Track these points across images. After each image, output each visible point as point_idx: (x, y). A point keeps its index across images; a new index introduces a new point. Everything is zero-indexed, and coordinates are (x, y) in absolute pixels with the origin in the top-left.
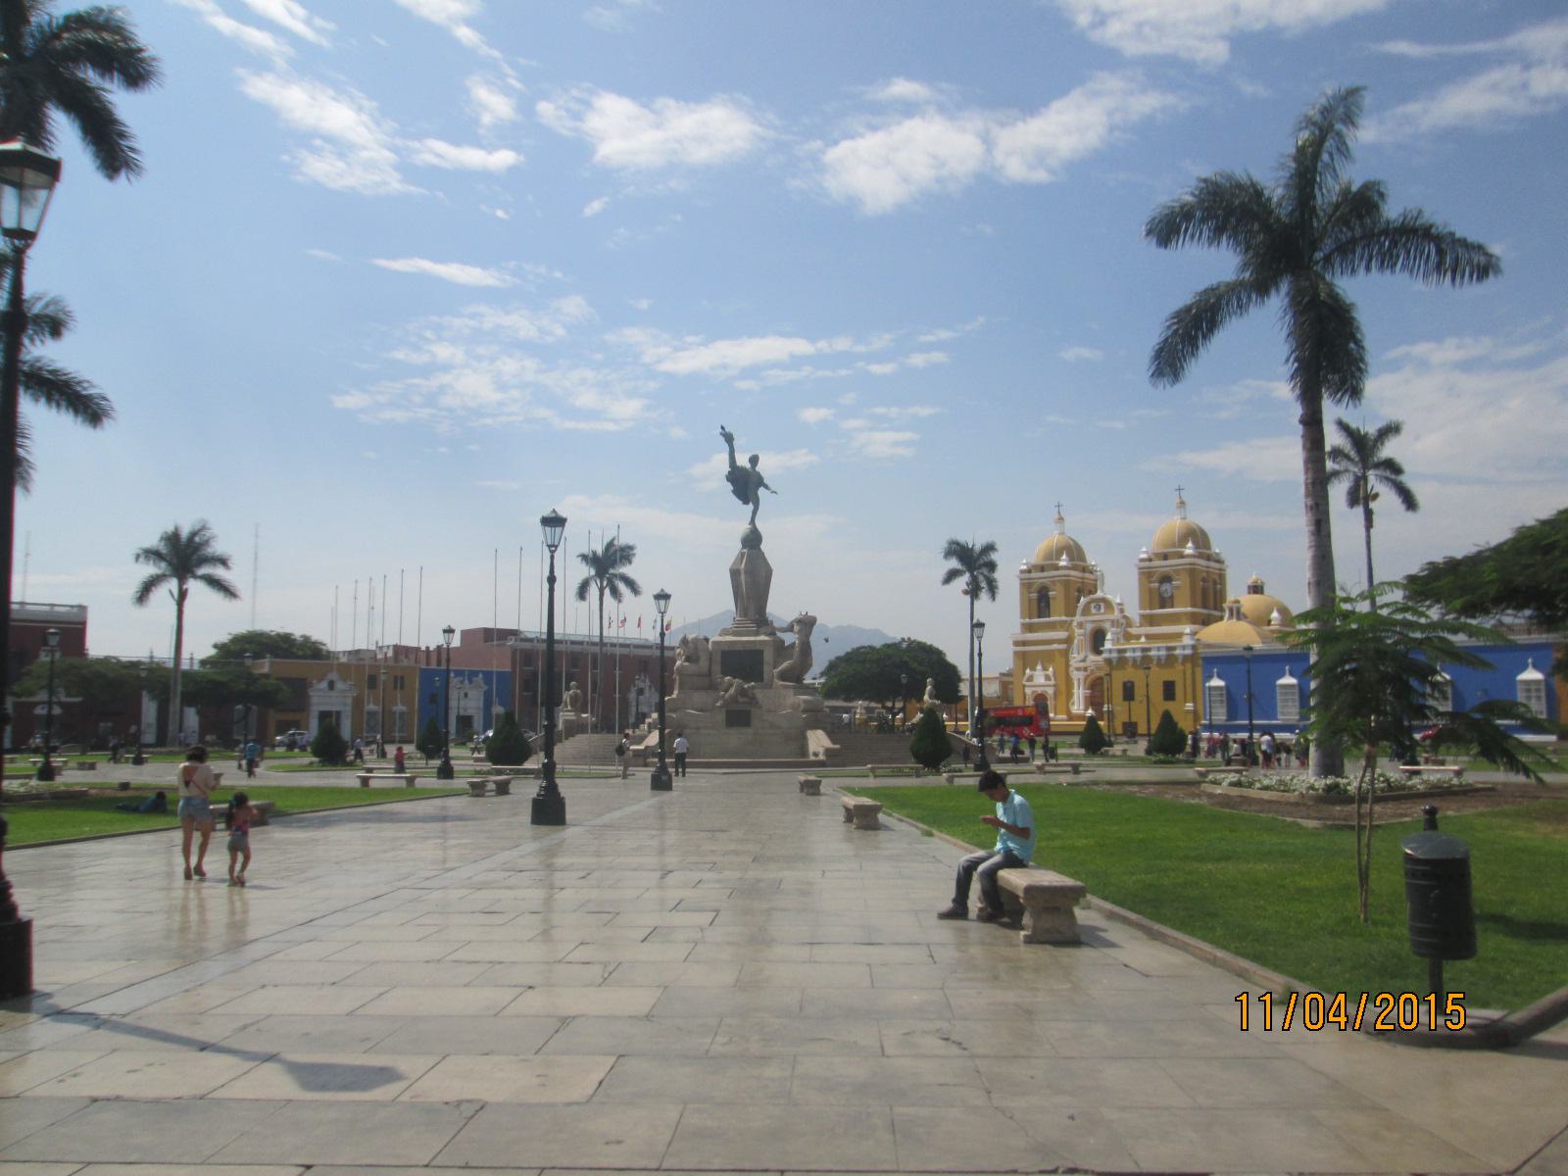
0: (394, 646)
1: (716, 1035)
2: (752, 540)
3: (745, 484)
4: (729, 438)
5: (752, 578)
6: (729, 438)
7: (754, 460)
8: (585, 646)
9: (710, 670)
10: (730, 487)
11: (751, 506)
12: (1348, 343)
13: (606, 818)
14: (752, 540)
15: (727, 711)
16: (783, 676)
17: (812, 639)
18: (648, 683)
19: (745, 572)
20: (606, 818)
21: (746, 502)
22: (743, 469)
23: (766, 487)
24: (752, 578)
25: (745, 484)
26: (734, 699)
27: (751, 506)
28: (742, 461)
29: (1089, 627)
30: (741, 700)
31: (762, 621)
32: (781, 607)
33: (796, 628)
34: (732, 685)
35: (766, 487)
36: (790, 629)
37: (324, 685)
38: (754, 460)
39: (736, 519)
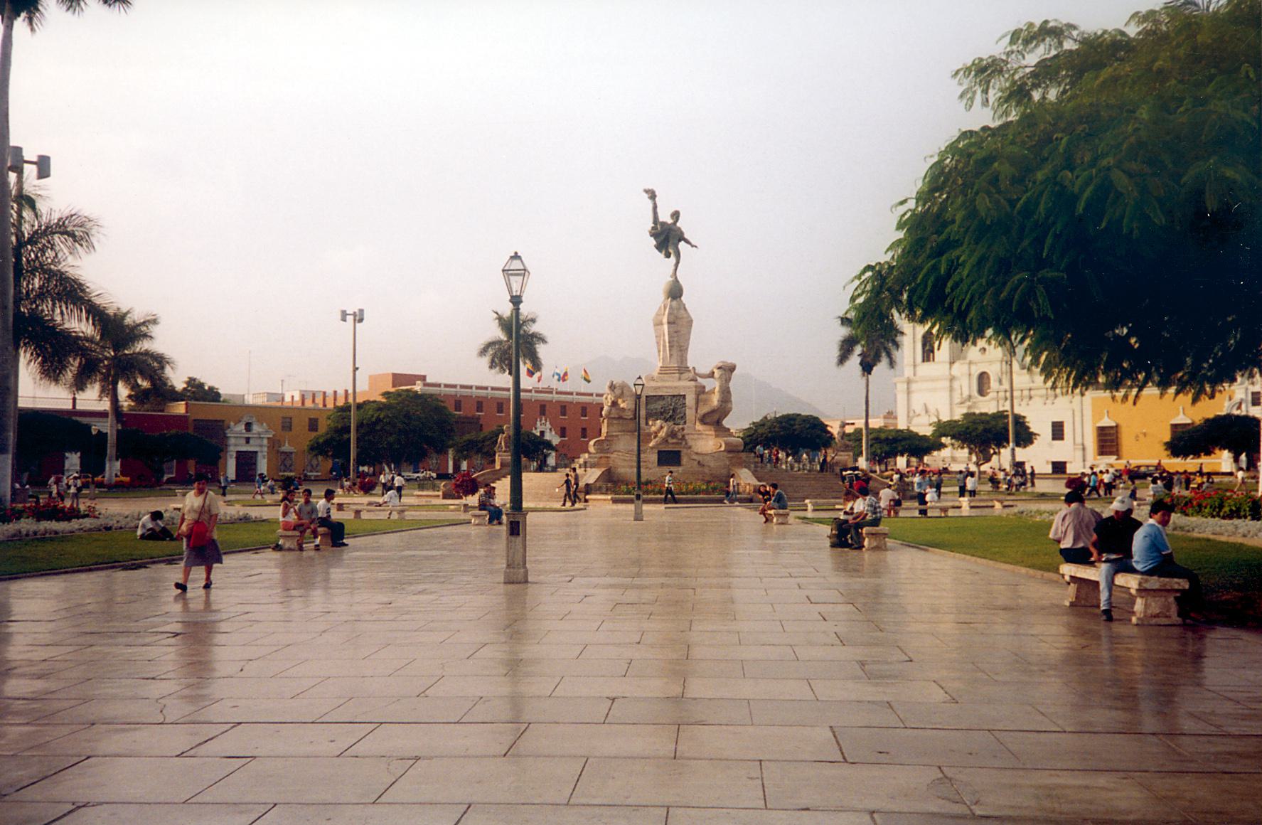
0: (57, 381)
1: (679, 715)
2: (675, 292)
3: (667, 237)
4: (652, 195)
5: (677, 325)
6: (652, 195)
7: (676, 215)
8: (442, 388)
9: (909, 392)
10: (653, 242)
11: (673, 259)
12: (1051, 103)
13: (39, 685)
14: (675, 292)
15: (659, 452)
16: (703, 420)
17: (731, 384)
18: (548, 425)
19: (1202, 380)
20: (39, 685)
21: (668, 255)
22: (663, 224)
23: (687, 242)
24: (677, 325)
25: (667, 237)
26: (665, 441)
27: (673, 259)
28: (665, 217)
29: (976, 371)
30: (671, 441)
31: (683, 369)
32: (702, 357)
33: (716, 375)
34: (659, 429)
35: (687, 242)
36: (712, 375)
37: (241, 427)
38: (676, 215)
39: (662, 267)
